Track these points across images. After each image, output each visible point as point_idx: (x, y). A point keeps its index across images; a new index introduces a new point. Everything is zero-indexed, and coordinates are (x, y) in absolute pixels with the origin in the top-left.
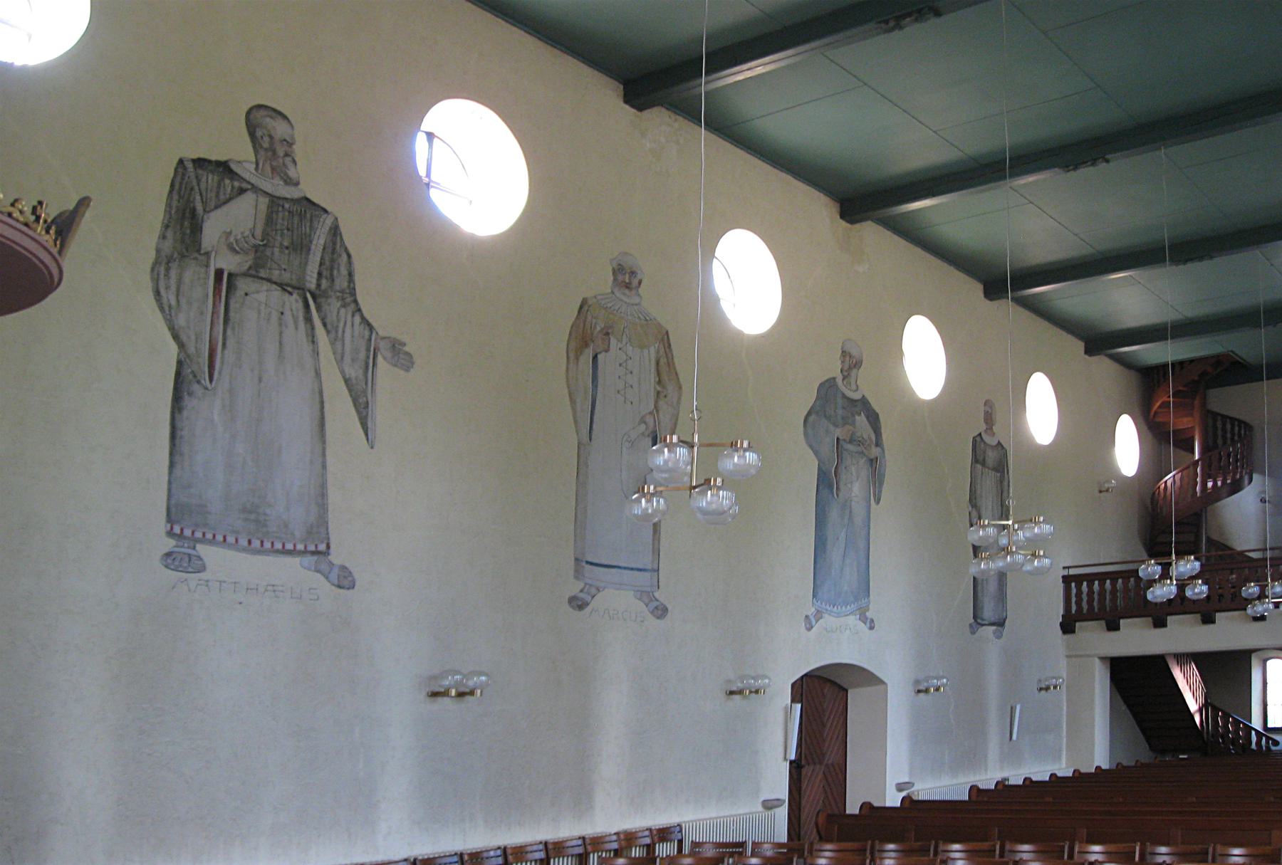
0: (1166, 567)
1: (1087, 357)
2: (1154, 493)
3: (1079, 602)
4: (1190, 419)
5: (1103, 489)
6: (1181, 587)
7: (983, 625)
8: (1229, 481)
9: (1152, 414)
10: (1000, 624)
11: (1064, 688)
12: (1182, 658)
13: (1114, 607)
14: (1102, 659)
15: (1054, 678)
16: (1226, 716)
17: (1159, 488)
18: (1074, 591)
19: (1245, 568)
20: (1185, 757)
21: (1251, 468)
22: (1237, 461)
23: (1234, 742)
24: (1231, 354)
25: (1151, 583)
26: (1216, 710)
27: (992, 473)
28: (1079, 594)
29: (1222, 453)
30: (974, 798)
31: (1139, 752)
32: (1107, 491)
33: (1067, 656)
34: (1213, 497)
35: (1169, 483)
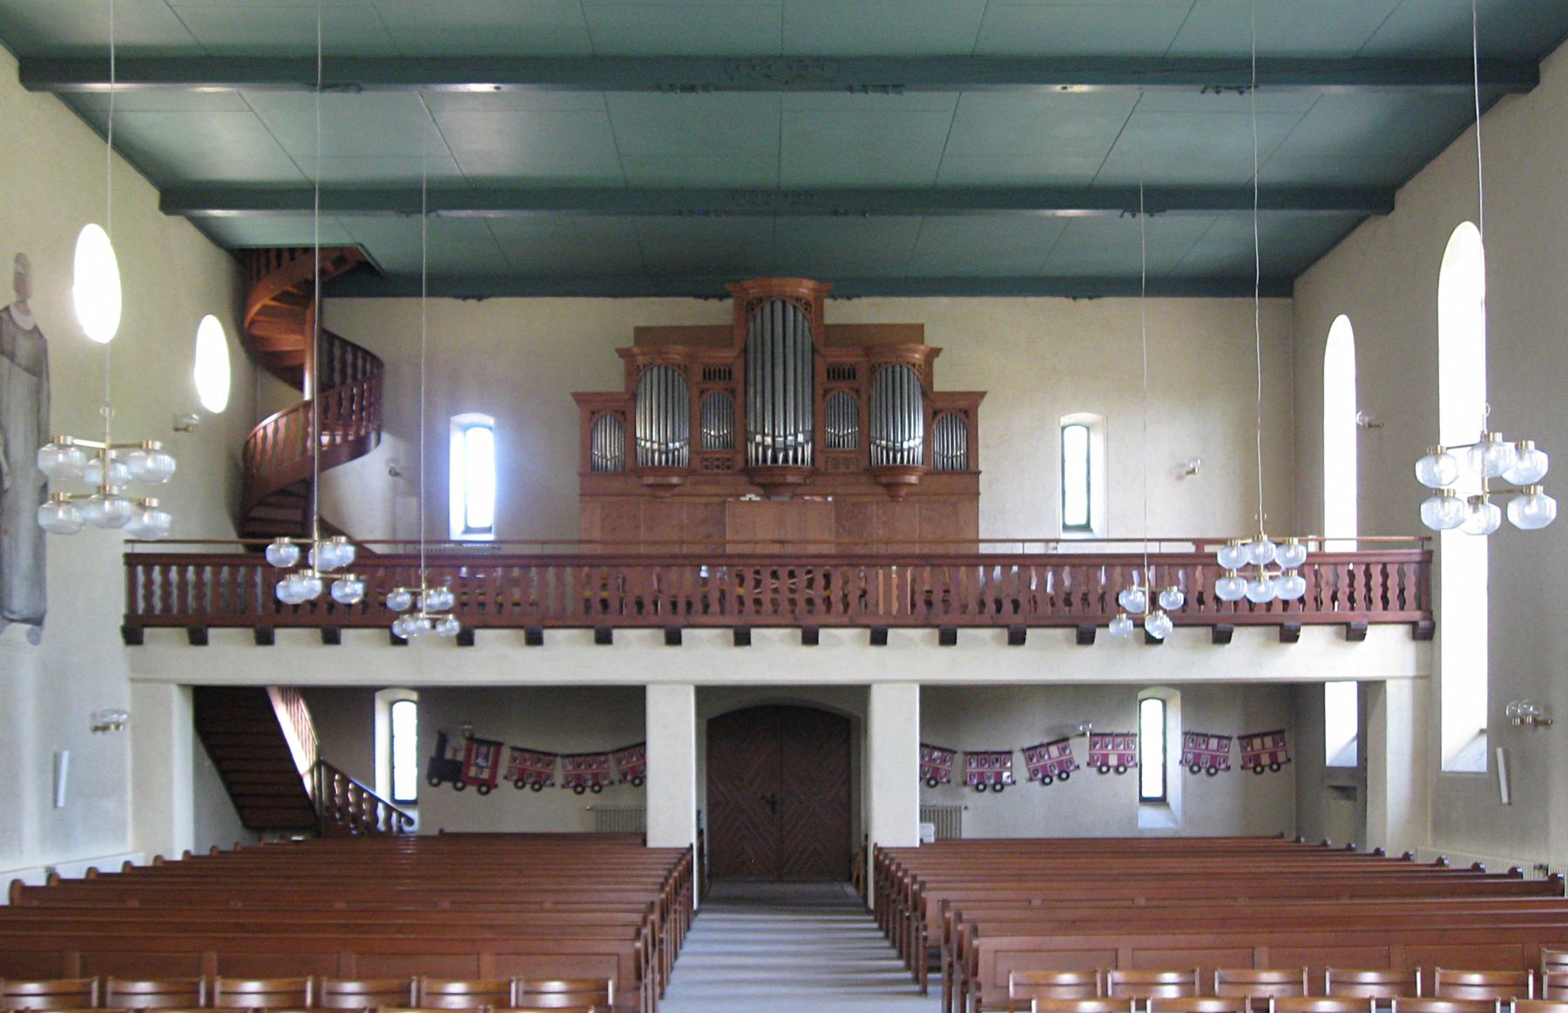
0: (305, 549)
1: (162, 215)
2: (248, 442)
3: (149, 596)
4: (300, 338)
5: (179, 426)
6: (328, 584)
7: (13, 621)
8: (351, 438)
9: (246, 325)
10: (37, 621)
11: (129, 726)
12: (294, 692)
13: (200, 609)
14: (183, 686)
15: (116, 712)
16: (345, 781)
17: (255, 435)
18: (141, 578)
19: (379, 566)
20: (300, 838)
21: (379, 422)
22: (362, 409)
23: (355, 818)
24: (359, 247)
25: (284, 573)
26: (332, 771)
27: (25, 376)
28: (149, 583)
29: (343, 394)
30: (17, 903)
31: (231, 835)
32: (186, 429)
33: (132, 680)
34: (331, 458)
35: (270, 431)
